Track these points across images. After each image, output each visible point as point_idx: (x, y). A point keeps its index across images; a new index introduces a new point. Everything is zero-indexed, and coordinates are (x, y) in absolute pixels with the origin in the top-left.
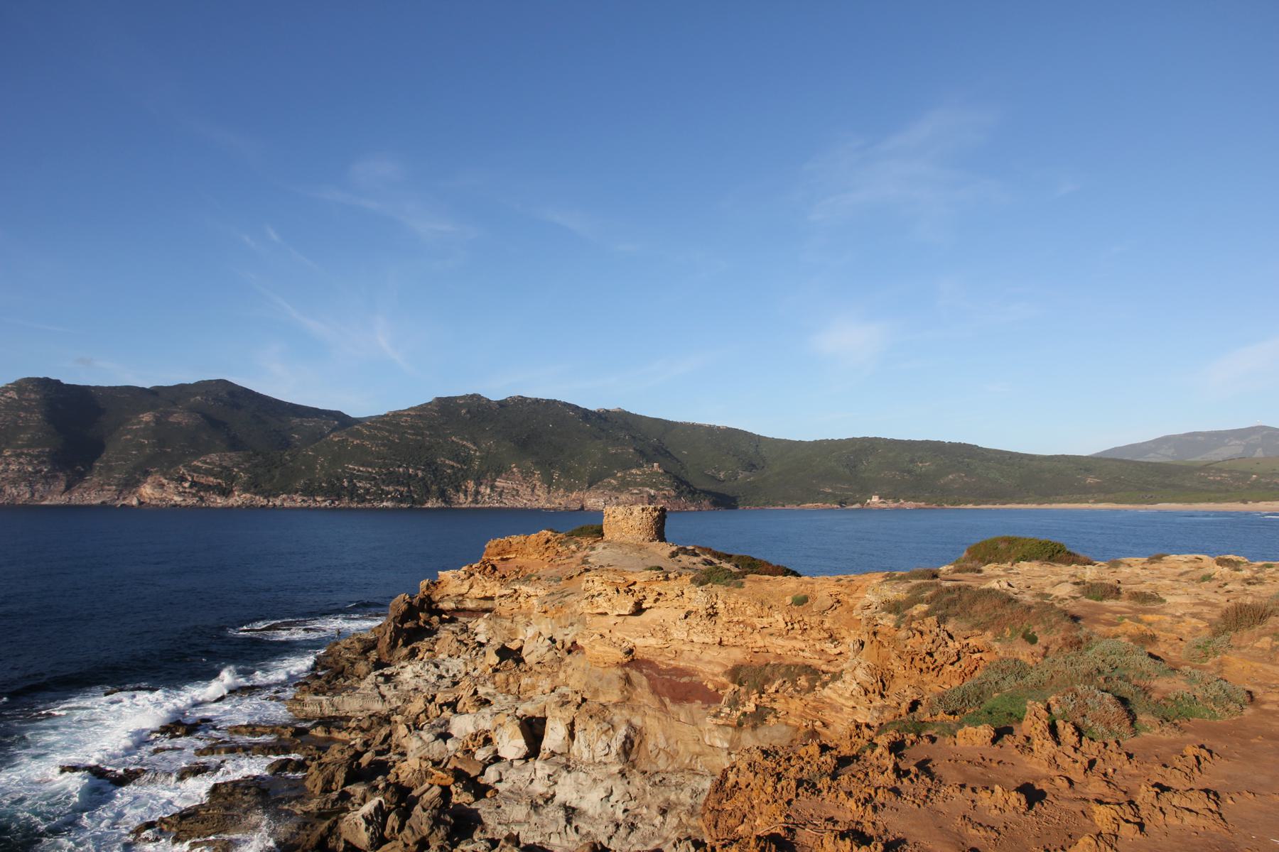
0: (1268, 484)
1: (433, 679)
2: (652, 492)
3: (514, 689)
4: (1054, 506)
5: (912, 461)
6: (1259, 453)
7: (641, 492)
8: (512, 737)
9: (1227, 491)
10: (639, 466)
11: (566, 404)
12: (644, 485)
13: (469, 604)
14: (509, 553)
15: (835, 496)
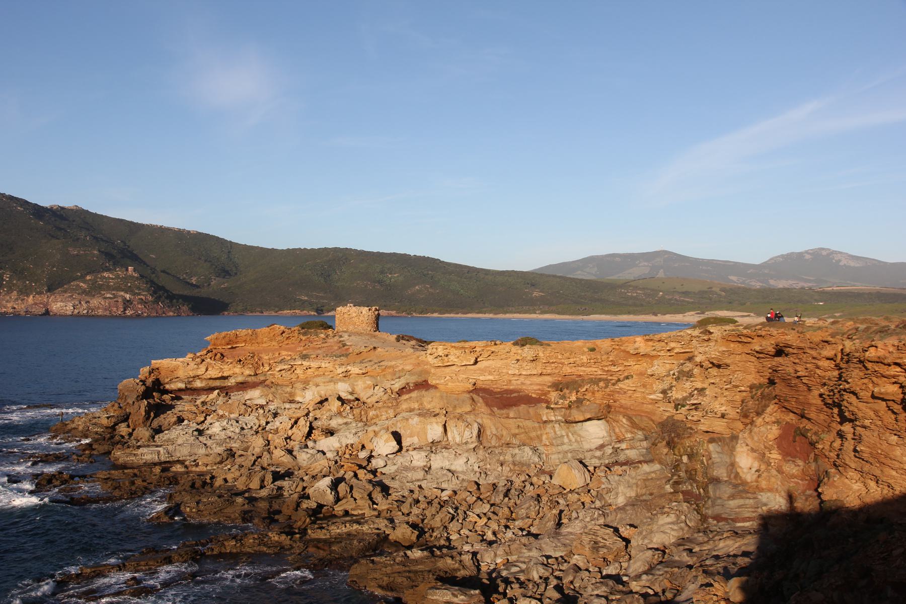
0: (670, 300)
1: (238, 430)
2: (128, 296)
3: (365, 419)
4: (508, 316)
5: (382, 272)
6: (661, 274)
7: (115, 296)
8: (386, 441)
9: (642, 305)
10: (108, 270)
11: (11, 198)
12: (119, 289)
13: (198, 384)
14: (236, 343)
15: (311, 304)
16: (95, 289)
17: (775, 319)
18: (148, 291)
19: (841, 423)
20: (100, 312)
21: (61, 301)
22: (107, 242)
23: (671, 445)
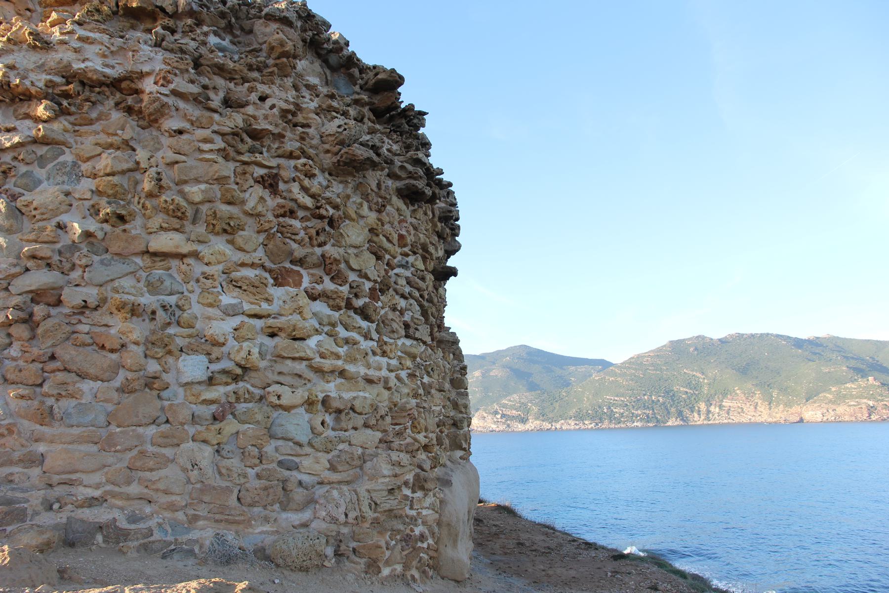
2: (871, 403)
10: (853, 381)
11: (778, 336)
12: (861, 397)
16: (840, 398)
17: (176, 40)
20: (847, 418)
21: (812, 410)
22: (856, 359)
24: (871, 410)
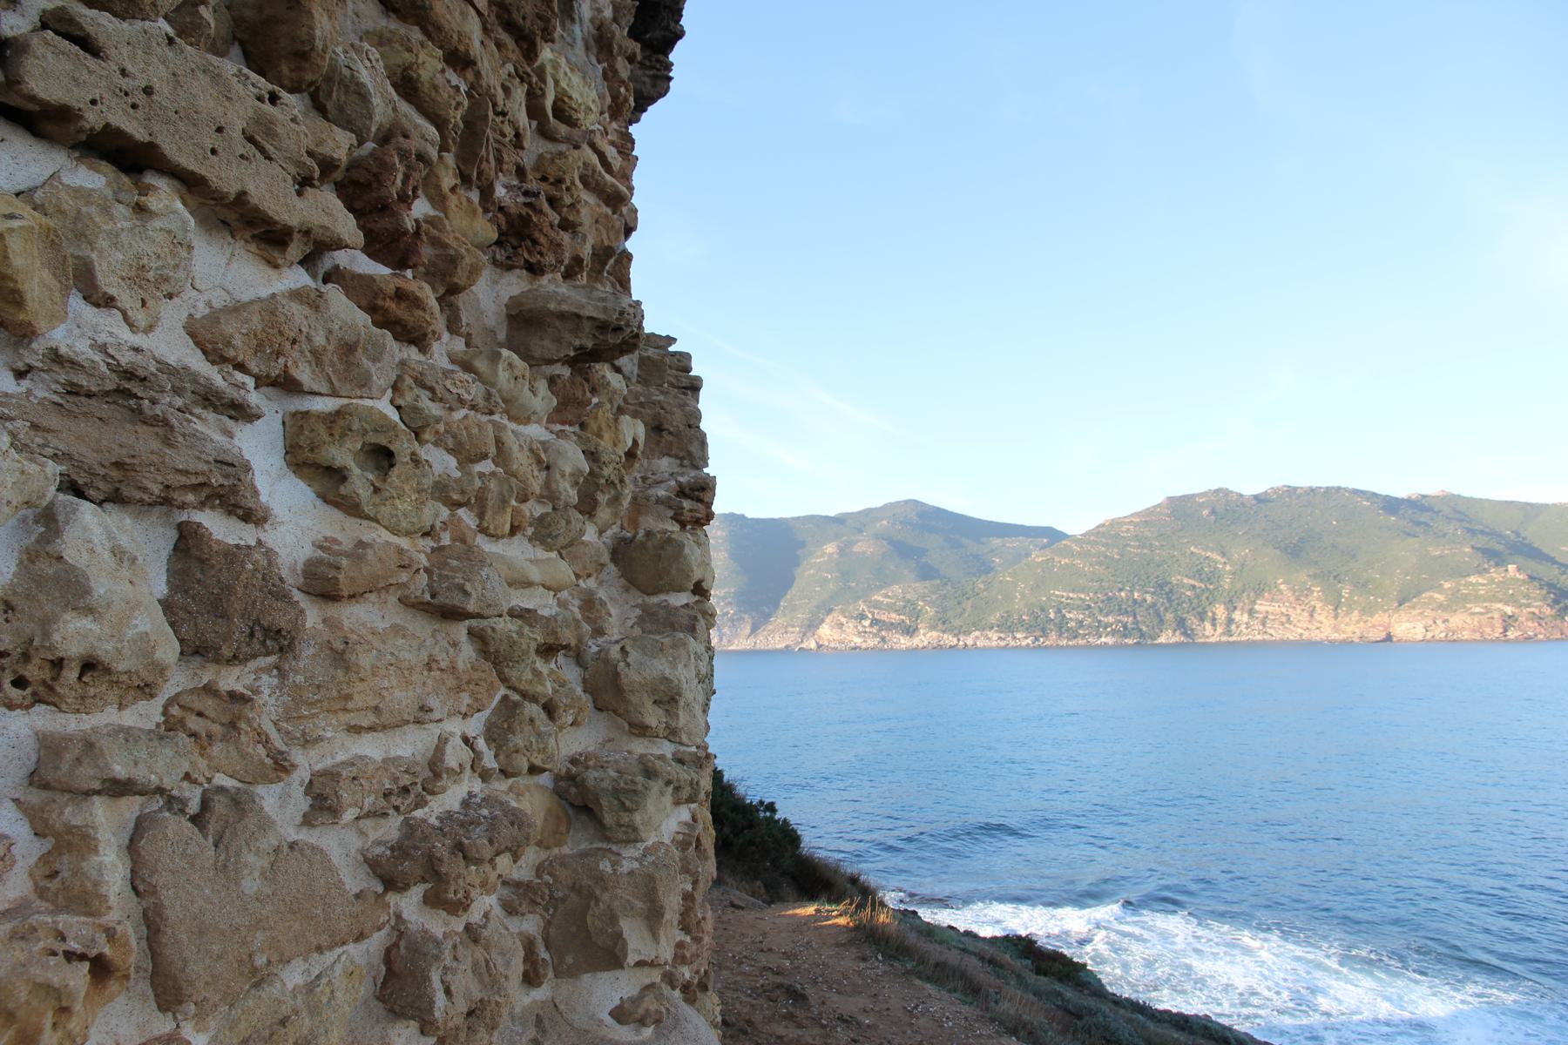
2: (1509, 610)
7: (1488, 611)
10: (1481, 571)
11: (1356, 492)
16: (1457, 602)
18: (1544, 599)
19: (34, 694)
20: (1466, 635)
22: (1489, 534)
23: (231, 1029)
24: (1508, 622)
